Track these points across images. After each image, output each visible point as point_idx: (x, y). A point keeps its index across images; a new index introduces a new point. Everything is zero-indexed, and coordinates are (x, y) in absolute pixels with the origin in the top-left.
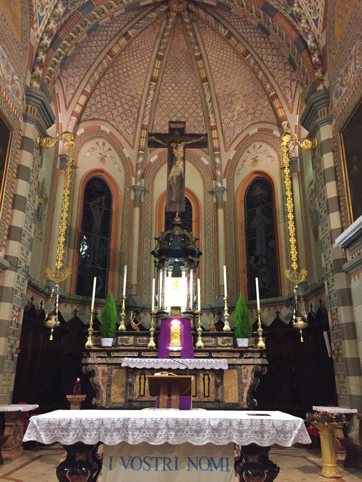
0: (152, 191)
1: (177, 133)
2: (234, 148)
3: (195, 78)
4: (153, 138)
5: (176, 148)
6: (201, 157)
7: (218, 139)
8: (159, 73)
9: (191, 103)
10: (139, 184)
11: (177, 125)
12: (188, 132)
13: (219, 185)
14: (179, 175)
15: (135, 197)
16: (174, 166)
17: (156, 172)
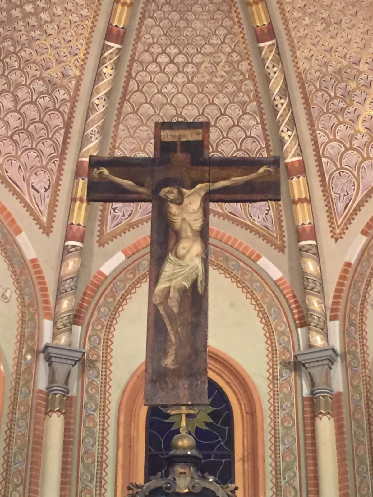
0: (106, 362)
1: (181, 156)
2: (362, 226)
3: (236, 29)
4: (105, 171)
5: (179, 202)
6: (259, 257)
7: (309, 202)
8: (131, 17)
9: (226, 100)
10: (63, 340)
11: (182, 132)
12: (216, 155)
13: (318, 340)
14: (187, 284)
15: (52, 379)
16: (171, 257)
17: (120, 304)
